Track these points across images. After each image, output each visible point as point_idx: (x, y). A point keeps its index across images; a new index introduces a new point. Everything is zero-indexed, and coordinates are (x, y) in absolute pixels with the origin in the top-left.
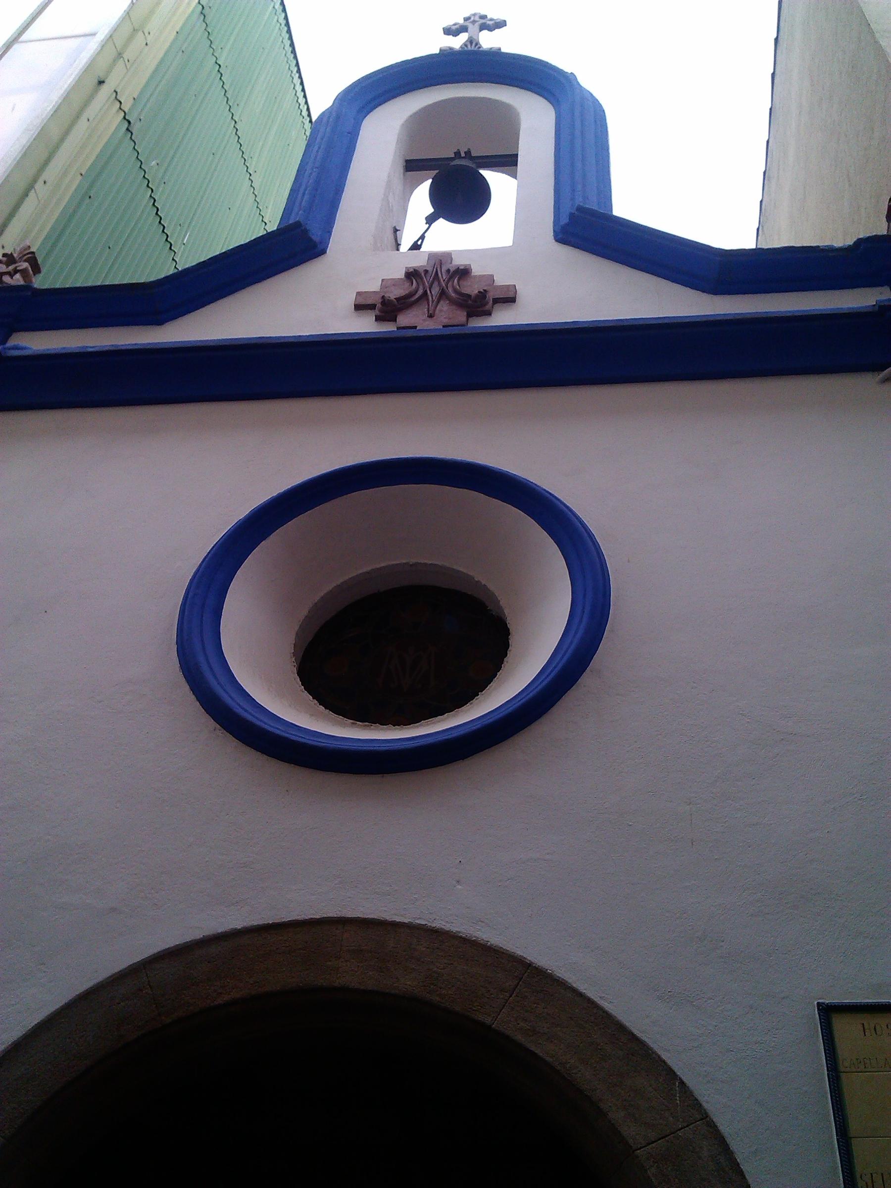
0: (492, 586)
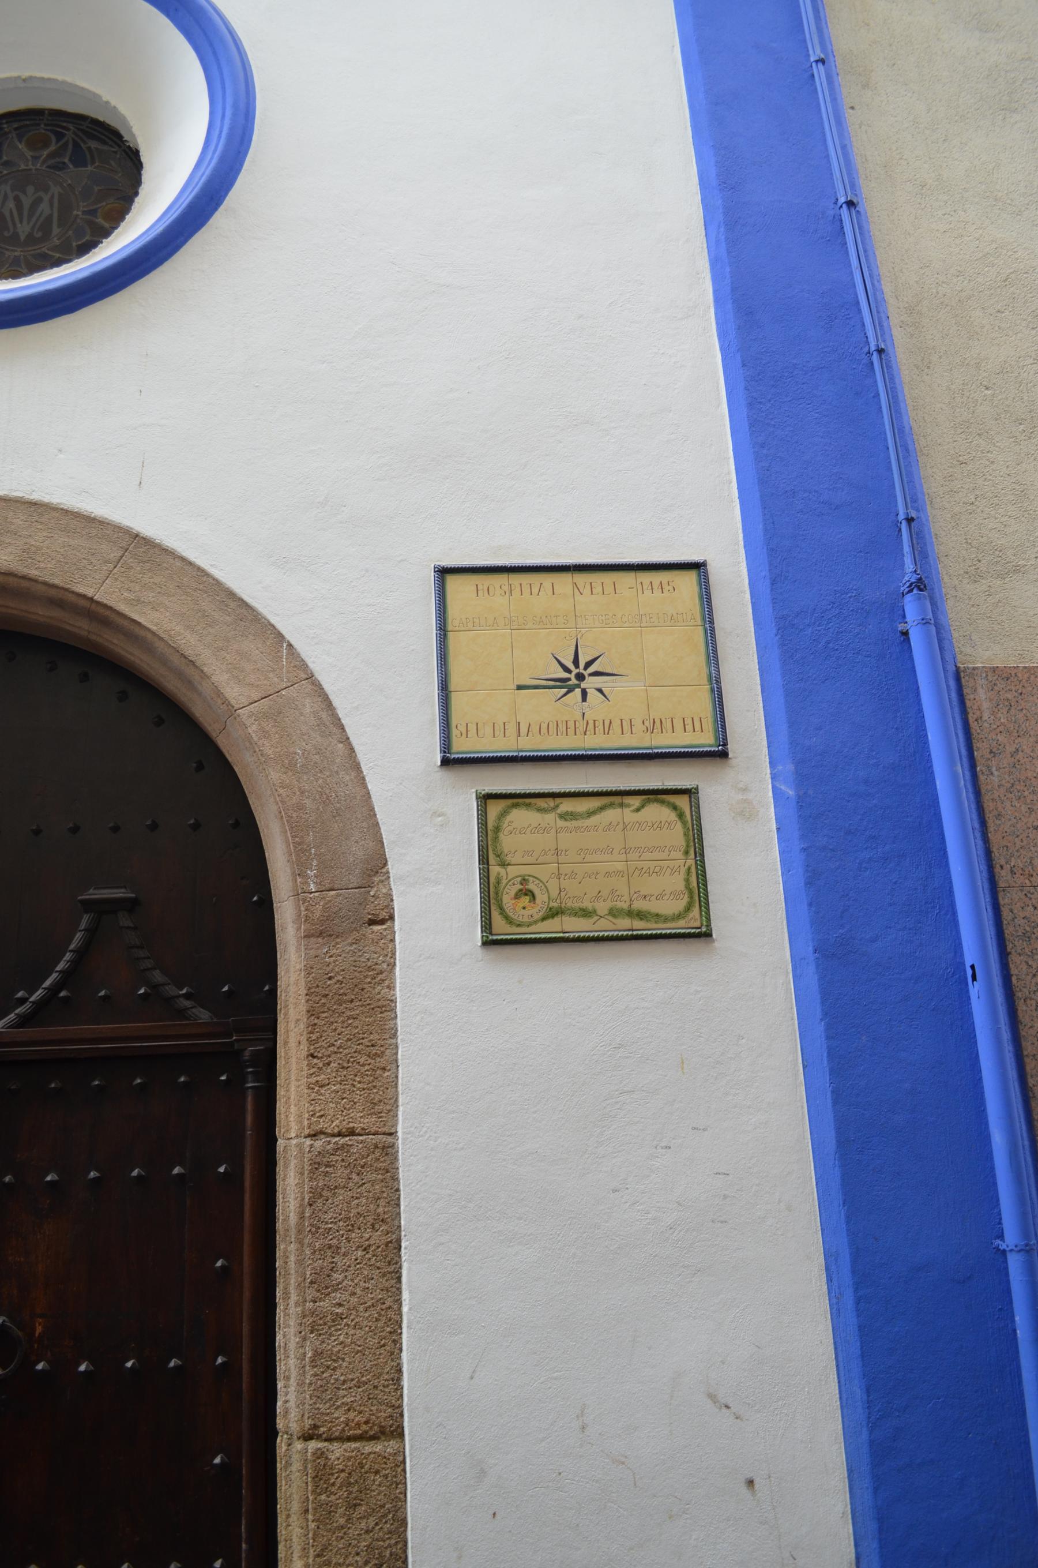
0: (123, 109)
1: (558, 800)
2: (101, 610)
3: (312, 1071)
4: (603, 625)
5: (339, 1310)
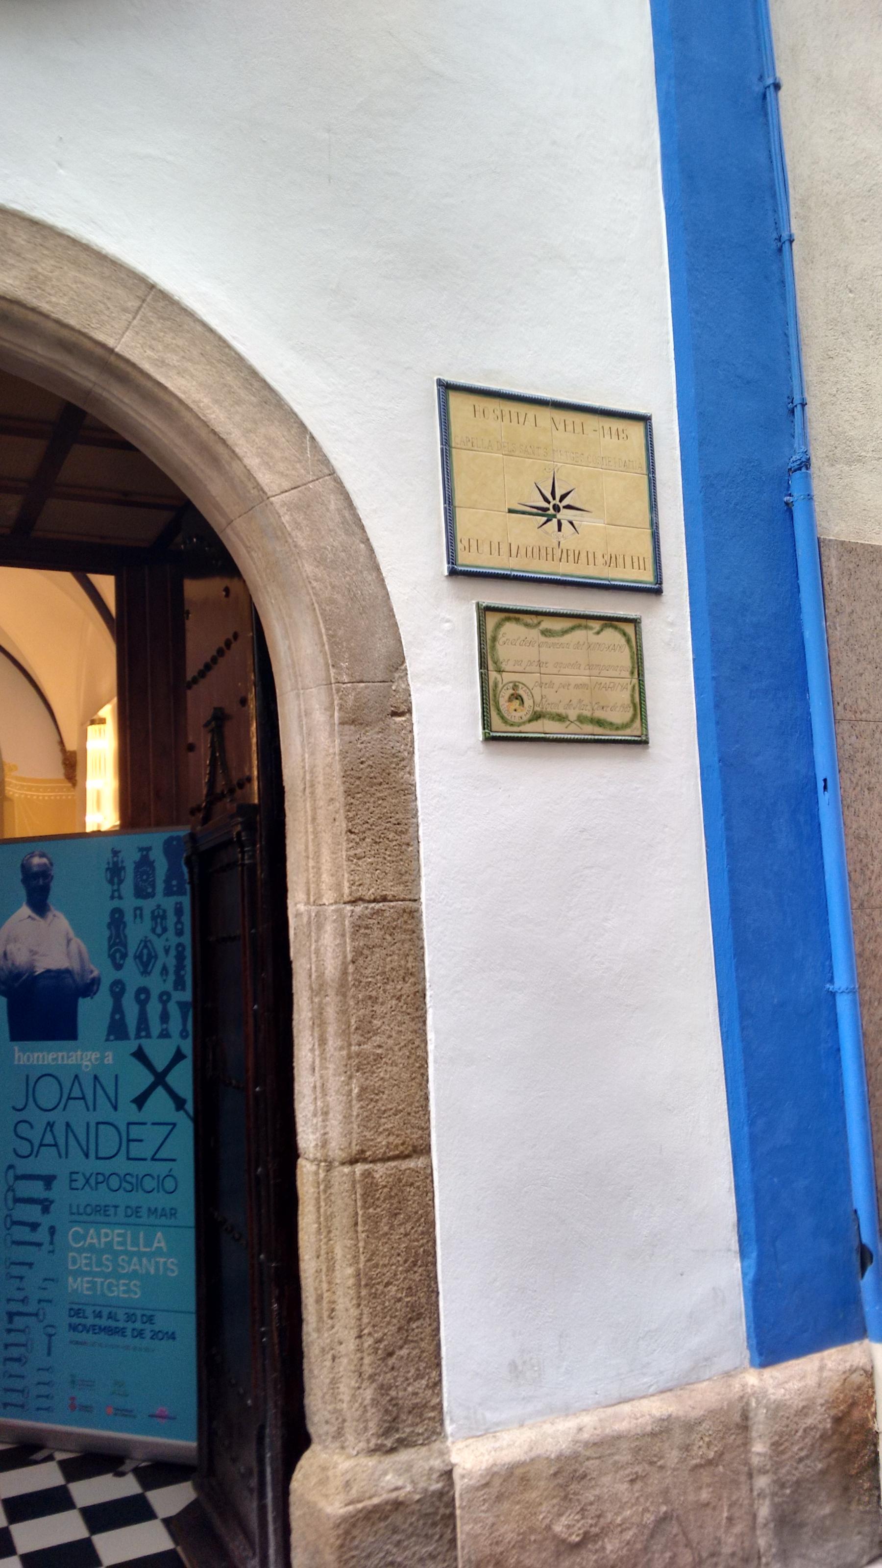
1: (540, 618)
2: (122, 365)
3: (351, 845)
4: (574, 462)
5: (379, 1051)
